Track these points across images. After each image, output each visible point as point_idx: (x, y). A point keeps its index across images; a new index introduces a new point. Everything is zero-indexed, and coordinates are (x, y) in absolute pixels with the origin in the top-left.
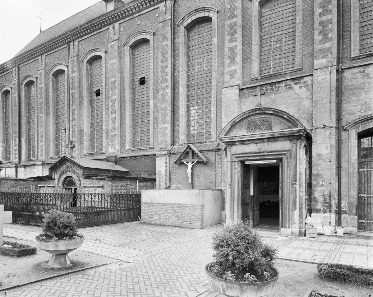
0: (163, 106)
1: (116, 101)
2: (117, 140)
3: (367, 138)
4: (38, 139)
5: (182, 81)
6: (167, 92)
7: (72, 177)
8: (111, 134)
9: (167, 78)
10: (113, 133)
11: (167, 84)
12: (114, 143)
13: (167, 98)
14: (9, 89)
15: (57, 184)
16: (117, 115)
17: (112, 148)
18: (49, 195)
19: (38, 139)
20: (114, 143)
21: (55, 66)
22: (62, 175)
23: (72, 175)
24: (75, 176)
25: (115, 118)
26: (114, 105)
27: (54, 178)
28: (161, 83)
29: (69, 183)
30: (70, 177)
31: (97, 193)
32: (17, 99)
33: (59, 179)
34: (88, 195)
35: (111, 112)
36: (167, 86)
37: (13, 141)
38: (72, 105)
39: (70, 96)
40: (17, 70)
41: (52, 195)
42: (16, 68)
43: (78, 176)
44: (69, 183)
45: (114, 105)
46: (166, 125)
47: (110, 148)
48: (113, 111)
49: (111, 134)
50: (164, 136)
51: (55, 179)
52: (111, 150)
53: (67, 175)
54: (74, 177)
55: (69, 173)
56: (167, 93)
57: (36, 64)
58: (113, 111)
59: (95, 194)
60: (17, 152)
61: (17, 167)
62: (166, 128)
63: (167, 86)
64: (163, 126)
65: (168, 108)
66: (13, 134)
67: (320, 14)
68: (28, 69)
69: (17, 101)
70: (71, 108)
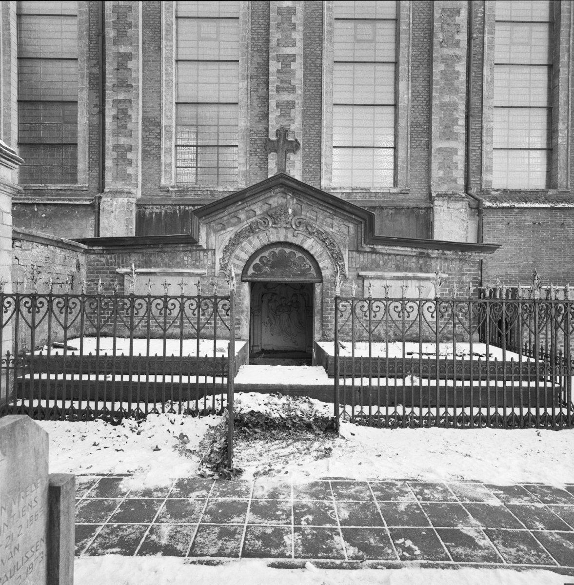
0: (447, 99)
1: (294, 60)
3: (109, 235)
5: (488, 54)
6: (457, 69)
9: (457, 37)
11: (458, 52)
13: (456, 82)
16: (297, 98)
26: (288, 69)
28: (442, 47)
31: (416, 295)
33: (229, 249)
34: (166, 303)
35: (278, 88)
36: (458, 58)
45: (288, 69)
46: (452, 144)
48: (285, 85)
50: (447, 166)
56: (458, 72)
58: (285, 85)
59: (34, 297)
62: (455, 151)
63: (458, 58)
64: (445, 145)
65: (460, 107)
67: (294, 60)
70: (111, 50)
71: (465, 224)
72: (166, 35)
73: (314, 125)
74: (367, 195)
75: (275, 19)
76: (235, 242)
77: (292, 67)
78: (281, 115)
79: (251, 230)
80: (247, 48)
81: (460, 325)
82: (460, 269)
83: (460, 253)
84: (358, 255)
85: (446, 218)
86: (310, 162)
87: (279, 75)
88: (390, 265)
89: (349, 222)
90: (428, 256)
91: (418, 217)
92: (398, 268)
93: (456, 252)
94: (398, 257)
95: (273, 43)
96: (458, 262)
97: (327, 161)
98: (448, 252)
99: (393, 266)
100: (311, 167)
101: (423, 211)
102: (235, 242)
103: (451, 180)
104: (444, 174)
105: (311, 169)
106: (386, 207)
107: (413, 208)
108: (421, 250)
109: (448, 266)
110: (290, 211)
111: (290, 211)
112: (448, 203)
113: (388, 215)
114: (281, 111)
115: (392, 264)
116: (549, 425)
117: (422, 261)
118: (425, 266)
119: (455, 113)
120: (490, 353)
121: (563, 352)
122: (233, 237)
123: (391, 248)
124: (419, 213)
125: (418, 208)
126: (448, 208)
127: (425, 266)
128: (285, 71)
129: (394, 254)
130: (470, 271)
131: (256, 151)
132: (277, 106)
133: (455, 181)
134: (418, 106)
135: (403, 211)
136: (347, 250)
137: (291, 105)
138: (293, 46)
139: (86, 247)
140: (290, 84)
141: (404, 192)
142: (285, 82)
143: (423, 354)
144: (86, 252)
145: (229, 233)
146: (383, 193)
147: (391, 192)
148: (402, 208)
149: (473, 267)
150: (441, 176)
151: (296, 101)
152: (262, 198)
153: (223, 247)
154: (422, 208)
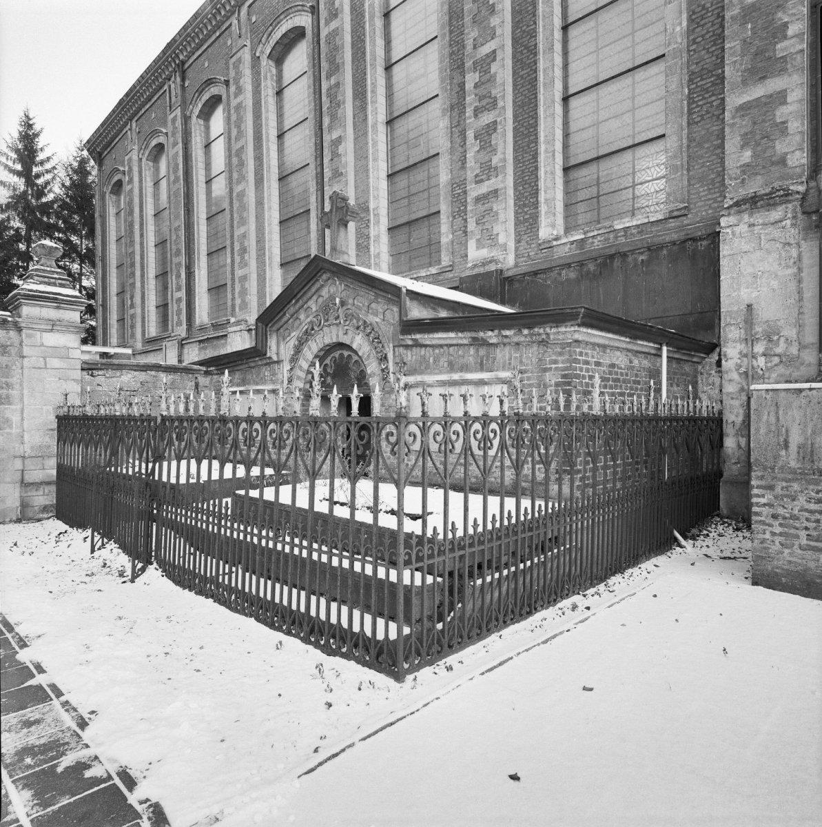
2: (506, 211)
4: (233, 261)
7: (349, 347)
8: (474, 191)
10: (484, 188)
12: (487, 226)
14: (162, 139)
15: (286, 382)
17: (480, 245)
18: (244, 425)
19: (233, 261)
20: (487, 226)
21: (276, 22)
22: (307, 340)
23: (346, 340)
24: (359, 342)
25: (492, 127)
26: (487, 76)
27: (275, 358)
29: (340, 367)
30: (341, 345)
32: (180, 160)
33: (294, 359)
37: (174, 277)
38: (330, 128)
39: (324, 98)
40: (178, 79)
41: (257, 425)
42: (177, 74)
43: (376, 340)
44: (340, 367)
47: (472, 244)
49: (474, 191)
51: (278, 362)
52: (475, 253)
53: (328, 341)
54: (354, 346)
55: (334, 329)
57: (226, 43)
58: (484, 102)
60: (183, 305)
61: (181, 346)
66: (173, 259)
68: (206, 65)
69: (181, 166)
71: (794, 253)
72: (372, 97)
73: (528, 146)
74: (612, 236)
75: (470, 11)
76: (298, 350)
77: (493, 71)
78: (482, 148)
79: (308, 334)
80: (446, 70)
81: (541, 466)
82: (540, 360)
83: (526, 332)
84: (405, 352)
85: (746, 247)
86: (525, 205)
87: (477, 91)
88: (441, 363)
89: (393, 304)
90: (485, 343)
91: (694, 257)
92: (452, 367)
93: (520, 330)
94: (451, 349)
95: (469, 43)
96: (535, 348)
97: (548, 196)
98: (507, 333)
99: (446, 365)
100: (526, 213)
101: (705, 243)
102: (298, 350)
103: (773, 164)
104: (755, 155)
105: (527, 217)
106: (633, 251)
107: (685, 241)
108: (474, 335)
109: (521, 356)
110: (338, 300)
111: (338, 300)
112: (751, 215)
113: (636, 265)
114: (480, 142)
115: (443, 362)
116: (344, 650)
117: (482, 352)
118: (487, 360)
119: (780, 15)
120: (429, 510)
121: (230, 506)
122: (296, 343)
123: (431, 336)
124: (695, 252)
125: (694, 240)
126: (751, 225)
127: (487, 360)
128: (487, 80)
129: (447, 345)
130: (555, 362)
131: (460, 210)
132: (476, 138)
133: (783, 161)
134: (703, 36)
135: (665, 252)
136: (391, 345)
137: (492, 127)
138: (493, 38)
139: (204, 369)
140: (490, 97)
141: (676, 213)
142: (485, 97)
143: (336, 503)
144: (207, 373)
145: (293, 342)
146: (638, 226)
147: (652, 219)
148: (661, 247)
149: (560, 354)
150: (748, 160)
151: (499, 120)
152: (313, 290)
153: (288, 357)
154: (701, 239)
